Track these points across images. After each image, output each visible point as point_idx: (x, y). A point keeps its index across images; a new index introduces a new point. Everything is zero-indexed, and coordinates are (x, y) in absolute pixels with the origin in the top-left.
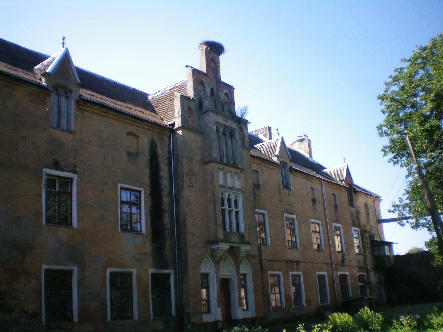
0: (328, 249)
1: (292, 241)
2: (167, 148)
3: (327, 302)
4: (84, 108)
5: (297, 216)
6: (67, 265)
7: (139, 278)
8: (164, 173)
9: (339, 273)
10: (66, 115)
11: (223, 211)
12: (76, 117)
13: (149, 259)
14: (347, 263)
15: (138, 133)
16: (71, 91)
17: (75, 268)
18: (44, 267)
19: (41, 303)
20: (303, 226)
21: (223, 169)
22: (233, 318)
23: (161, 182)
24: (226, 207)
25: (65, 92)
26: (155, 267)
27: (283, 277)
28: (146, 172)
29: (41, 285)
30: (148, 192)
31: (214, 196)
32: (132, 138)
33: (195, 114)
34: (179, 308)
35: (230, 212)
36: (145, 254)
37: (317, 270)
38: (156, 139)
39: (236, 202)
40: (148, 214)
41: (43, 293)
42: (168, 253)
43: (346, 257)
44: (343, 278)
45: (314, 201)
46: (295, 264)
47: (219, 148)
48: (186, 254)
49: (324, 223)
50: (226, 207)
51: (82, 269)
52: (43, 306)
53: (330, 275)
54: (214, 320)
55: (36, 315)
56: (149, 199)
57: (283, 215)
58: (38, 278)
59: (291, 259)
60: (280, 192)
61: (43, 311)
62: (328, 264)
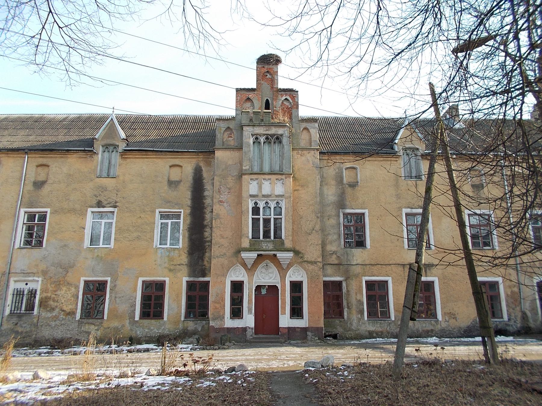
1: (22, 246)
3: (502, 318)
4: (126, 156)
13: (185, 270)
15: (181, 164)
16: (118, 146)
21: (257, 179)
26: (190, 276)
28: (188, 195)
30: (188, 211)
38: (202, 164)
41: (80, 297)
51: (114, 281)
54: (244, 326)
55: (72, 313)
58: (77, 287)
60: (397, 185)
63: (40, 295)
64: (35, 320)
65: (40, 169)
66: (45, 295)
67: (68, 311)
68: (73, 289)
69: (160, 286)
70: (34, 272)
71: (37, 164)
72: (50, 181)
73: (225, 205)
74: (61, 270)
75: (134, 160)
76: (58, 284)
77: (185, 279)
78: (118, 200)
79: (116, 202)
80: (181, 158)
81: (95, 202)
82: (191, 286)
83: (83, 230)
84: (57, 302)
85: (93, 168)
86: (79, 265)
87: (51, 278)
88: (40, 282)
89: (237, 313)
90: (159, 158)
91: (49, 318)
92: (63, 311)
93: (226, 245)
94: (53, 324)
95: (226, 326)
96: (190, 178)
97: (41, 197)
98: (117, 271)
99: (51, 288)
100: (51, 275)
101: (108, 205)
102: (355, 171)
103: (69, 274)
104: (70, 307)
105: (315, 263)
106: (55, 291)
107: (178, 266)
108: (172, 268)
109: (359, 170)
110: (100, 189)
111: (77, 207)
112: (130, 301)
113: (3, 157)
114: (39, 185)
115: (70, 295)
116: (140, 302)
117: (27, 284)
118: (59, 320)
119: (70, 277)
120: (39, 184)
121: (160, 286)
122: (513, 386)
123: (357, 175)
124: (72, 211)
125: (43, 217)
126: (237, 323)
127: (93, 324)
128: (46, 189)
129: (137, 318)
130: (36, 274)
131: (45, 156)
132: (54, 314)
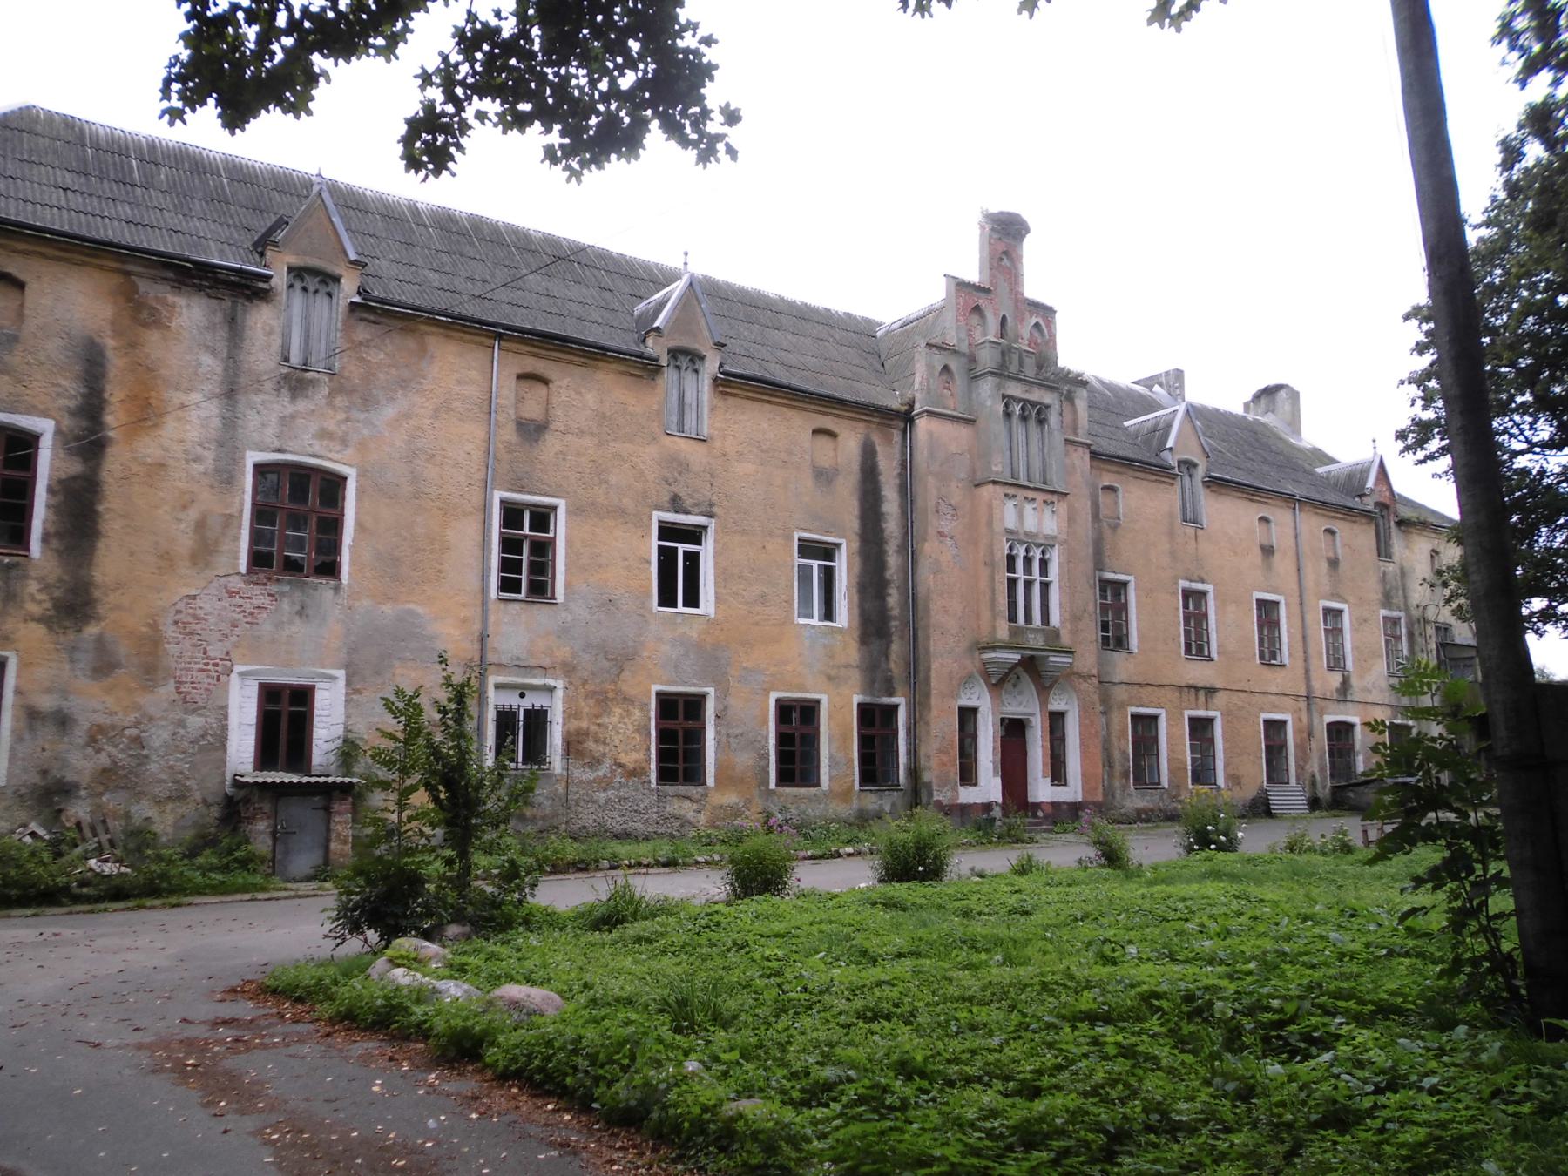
0: (1300, 663)
2: (898, 456)
4: (728, 390)
5: (1215, 585)
6: (695, 685)
7: (833, 707)
8: (891, 504)
9: (1329, 718)
10: (694, 405)
11: (1012, 583)
12: (712, 410)
13: (855, 677)
14: (1356, 695)
15: (22, 276)
17: (711, 691)
18: (655, 688)
19: (649, 749)
20: (1232, 608)
22: (1031, 800)
23: (884, 526)
24: (1020, 573)
25: (692, 361)
26: (863, 693)
27: (1167, 720)
29: (650, 719)
30: (856, 545)
31: (992, 553)
32: (823, 441)
33: (958, 382)
34: (914, 772)
35: (1028, 584)
36: (847, 666)
37: (1262, 710)
39: (1044, 564)
40: (854, 591)
42: (895, 665)
43: (1354, 681)
44: (1341, 732)
45: (1268, 551)
46: (1202, 694)
47: (1011, 449)
48: (929, 669)
49: (1295, 600)
50: (1020, 573)
51: (722, 695)
52: (653, 756)
53: (1300, 720)
54: (985, 801)
56: (857, 560)
57: (1177, 583)
59: (1191, 682)
60: (1171, 534)
61: (653, 766)
62: (1296, 697)
63: (564, 724)
64: (560, 789)
65: (525, 384)
66: (574, 725)
67: (631, 766)
68: (637, 714)
69: (809, 711)
70: (544, 665)
71: (520, 371)
72: (555, 425)
73: (948, 541)
74: (606, 664)
75: (744, 401)
76: (603, 701)
77: (856, 699)
78: (715, 498)
79: (711, 505)
80: (839, 416)
81: (666, 498)
82: (866, 712)
83: (646, 566)
84: (605, 743)
85: (655, 407)
86: (645, 654)
87: (585, 682)
88: (559, 693)
89: (968, 775)
90: (795, 408)
91: (589, 783)
92: (621, 766)
93: (953, 632)
94: (601, 796)
95: (959, 801)
96: (855, 466)
97: (539, 466)
98: (726, 673)
99: (586, 707)
100: (585, 675)
101: (696, 510)
102: (1112, 495)
103: (626, 675)
104: (634, 756)
105: (1090, 676)
106: (597, 717)
107: (843, 670)
108: (833, 673)
109: (1120, 494)
110: (675, 464)
111: (628, 503)
112: (757, 745)
113: (433, 334)
114: (531, 430)
115: (630, 727)
116: (707, 744)
117: (522, 695)
118: (613, 788)
119: (629, 683)
120: (532, 428)
121: (809, 711)
122: (394, 997)
123: (1116, 503)
124: (620, 513)
125: (542, 518)
126: (967, 795)
127: (688, 798)
128: (551, 444)
129: (772, 785)
130: (549, 671)
131: (544, 352)
132: (601, 774)
